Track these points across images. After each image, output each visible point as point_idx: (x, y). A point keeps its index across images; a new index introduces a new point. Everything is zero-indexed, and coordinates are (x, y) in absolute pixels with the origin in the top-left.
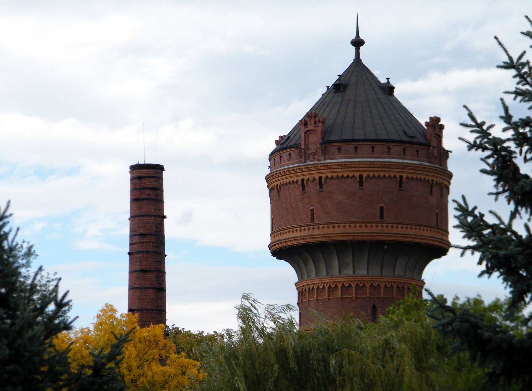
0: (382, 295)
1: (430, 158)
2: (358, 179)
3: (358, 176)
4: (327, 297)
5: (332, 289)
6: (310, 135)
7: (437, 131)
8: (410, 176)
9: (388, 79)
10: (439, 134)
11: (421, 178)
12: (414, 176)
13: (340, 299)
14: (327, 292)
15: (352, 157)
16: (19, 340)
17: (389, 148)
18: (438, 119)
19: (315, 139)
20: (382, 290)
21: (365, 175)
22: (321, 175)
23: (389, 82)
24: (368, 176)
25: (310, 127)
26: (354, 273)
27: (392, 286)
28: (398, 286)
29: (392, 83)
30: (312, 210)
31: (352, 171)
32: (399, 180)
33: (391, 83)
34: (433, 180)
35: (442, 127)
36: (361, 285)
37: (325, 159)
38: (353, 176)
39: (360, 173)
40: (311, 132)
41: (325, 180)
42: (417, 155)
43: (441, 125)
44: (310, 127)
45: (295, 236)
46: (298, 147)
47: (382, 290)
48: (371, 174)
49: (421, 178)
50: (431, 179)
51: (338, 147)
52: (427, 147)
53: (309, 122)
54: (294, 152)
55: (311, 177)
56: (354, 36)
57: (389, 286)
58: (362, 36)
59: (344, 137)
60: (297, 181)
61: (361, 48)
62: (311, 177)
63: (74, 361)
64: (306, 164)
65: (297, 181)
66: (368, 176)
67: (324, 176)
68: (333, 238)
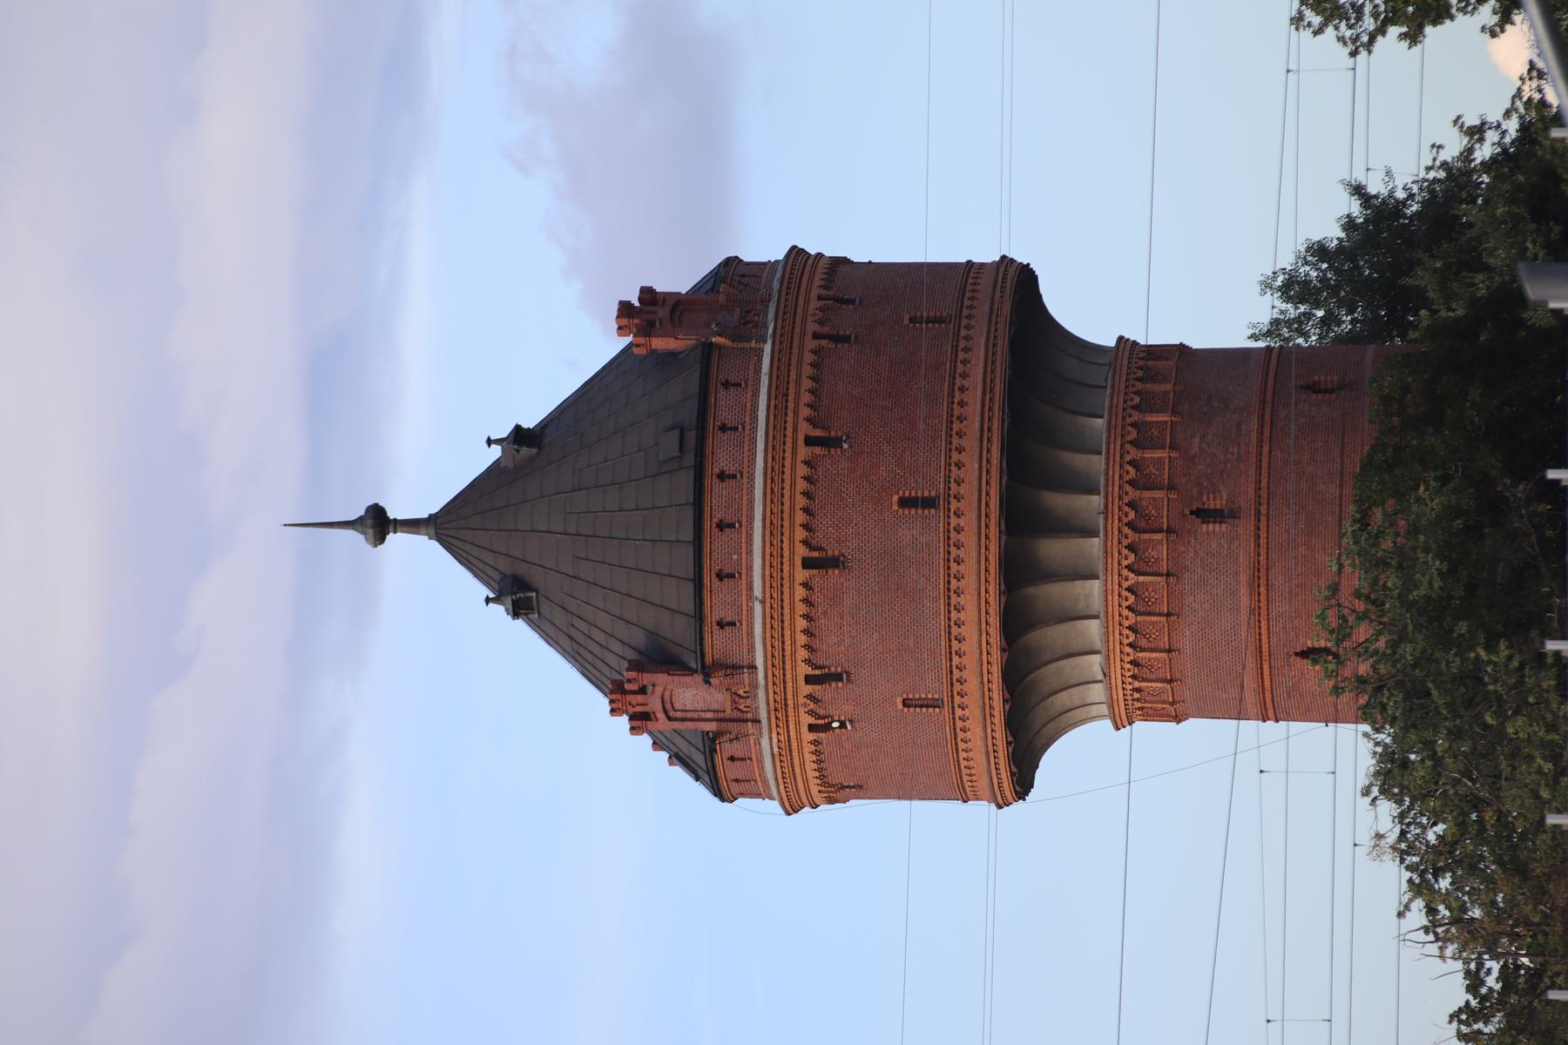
0: (1168, 387)
1: (746, 328)
4: (1163, 619)
5: (1140, 603)
6: (677, 706)
7: (663, 312)
8: (805, 412)
9: (489, 442)
10: (671, 302)
11: (811, 365)
13: (1173, 537)
14: (1146, 494)
15: (751, 634)
17: (721, 526)
18: (625, 309)
19: (690, 694)
20: (1150, 418)
21: (805, 429)
22: (801, 437)
23: (498, 442)
25: (654, 704)
26: (1098, 652)
29: (504, 431)
30: (906, 703)
31: (792, 497)
32: (818, 450)
33: (505, 435)
37: (753, 667)
38: (805, 585)
39: (801, 443)
40: (668, 706)
41: (812, 549)
42: (742, 385)
45: (983, 735)
46: (713, 740)
47: (1150, 418)
50: (814, 304)
51: (716, 627)
52: (715, 353)
53: (639, 709)
54: (726, 748)
55: (805, 705)
56: (354, 538)
59: (688, 606)
60: (816, 742)
61: (391, 515)
62: (805, 705)
64: (764, 721)
65: (816, 742)
68: (991, 578)
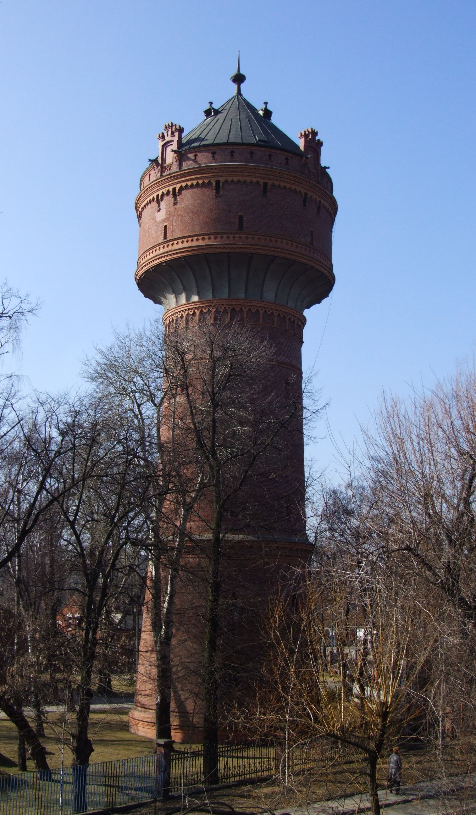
2: (262, 187)
3: (262, 183)
12: (293, 187)
16: (395, 758)
21: (222, 179)
24: (273, 185)
27: (284, 316)
28: (279, 315)
34: (306, 194)
35: (320, 144)
36: (269, 313)
43: (319, 140)
44: (167, 139)
48: (229, 179)
49: (295, 189)
56: (235, 72)
57: (282, 316)
58: (242, 72)
63: (85, 422)
66: (226, 181)
67: (222, 179)
